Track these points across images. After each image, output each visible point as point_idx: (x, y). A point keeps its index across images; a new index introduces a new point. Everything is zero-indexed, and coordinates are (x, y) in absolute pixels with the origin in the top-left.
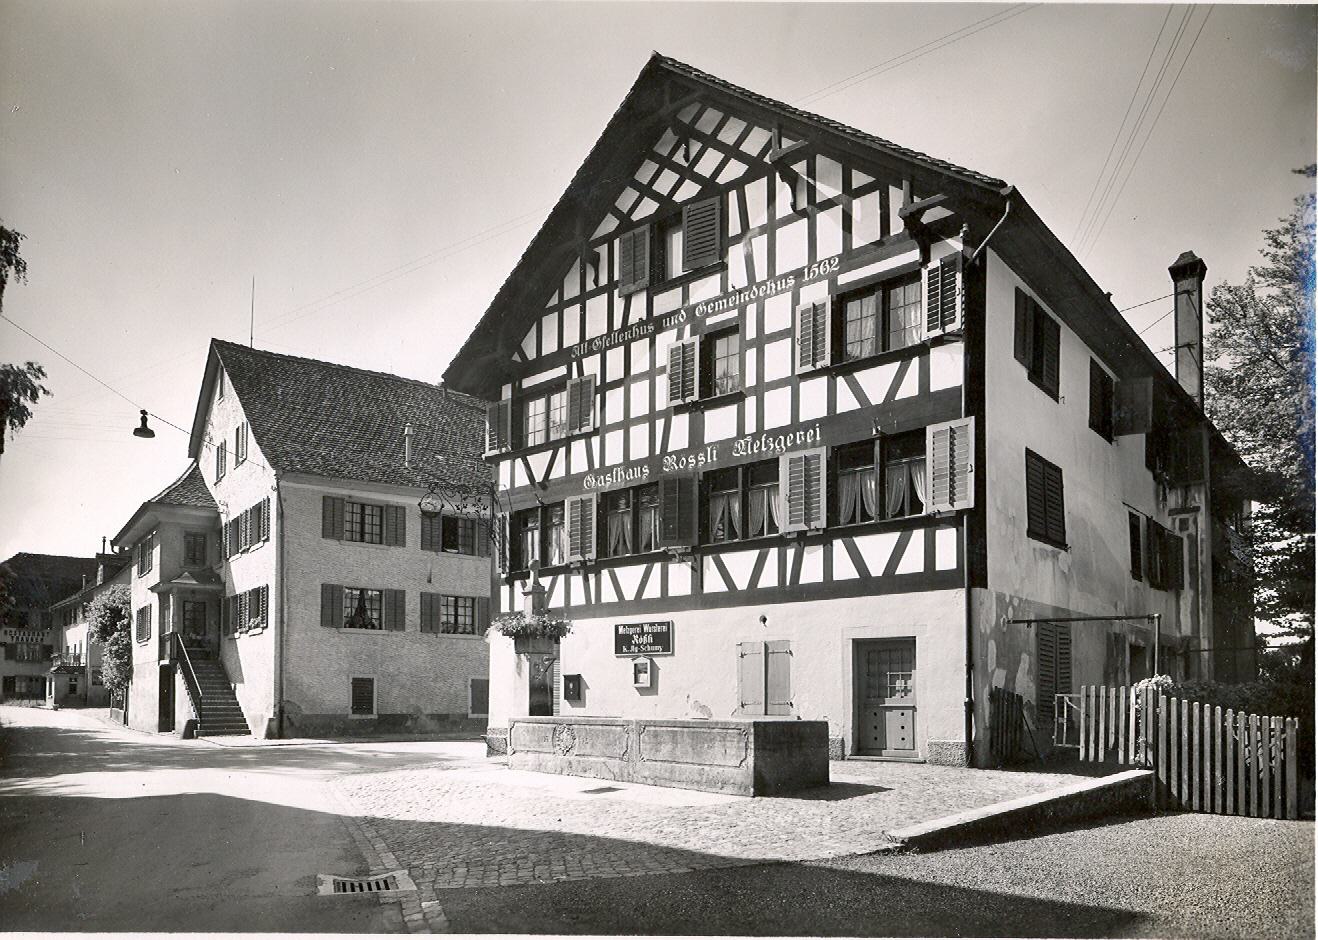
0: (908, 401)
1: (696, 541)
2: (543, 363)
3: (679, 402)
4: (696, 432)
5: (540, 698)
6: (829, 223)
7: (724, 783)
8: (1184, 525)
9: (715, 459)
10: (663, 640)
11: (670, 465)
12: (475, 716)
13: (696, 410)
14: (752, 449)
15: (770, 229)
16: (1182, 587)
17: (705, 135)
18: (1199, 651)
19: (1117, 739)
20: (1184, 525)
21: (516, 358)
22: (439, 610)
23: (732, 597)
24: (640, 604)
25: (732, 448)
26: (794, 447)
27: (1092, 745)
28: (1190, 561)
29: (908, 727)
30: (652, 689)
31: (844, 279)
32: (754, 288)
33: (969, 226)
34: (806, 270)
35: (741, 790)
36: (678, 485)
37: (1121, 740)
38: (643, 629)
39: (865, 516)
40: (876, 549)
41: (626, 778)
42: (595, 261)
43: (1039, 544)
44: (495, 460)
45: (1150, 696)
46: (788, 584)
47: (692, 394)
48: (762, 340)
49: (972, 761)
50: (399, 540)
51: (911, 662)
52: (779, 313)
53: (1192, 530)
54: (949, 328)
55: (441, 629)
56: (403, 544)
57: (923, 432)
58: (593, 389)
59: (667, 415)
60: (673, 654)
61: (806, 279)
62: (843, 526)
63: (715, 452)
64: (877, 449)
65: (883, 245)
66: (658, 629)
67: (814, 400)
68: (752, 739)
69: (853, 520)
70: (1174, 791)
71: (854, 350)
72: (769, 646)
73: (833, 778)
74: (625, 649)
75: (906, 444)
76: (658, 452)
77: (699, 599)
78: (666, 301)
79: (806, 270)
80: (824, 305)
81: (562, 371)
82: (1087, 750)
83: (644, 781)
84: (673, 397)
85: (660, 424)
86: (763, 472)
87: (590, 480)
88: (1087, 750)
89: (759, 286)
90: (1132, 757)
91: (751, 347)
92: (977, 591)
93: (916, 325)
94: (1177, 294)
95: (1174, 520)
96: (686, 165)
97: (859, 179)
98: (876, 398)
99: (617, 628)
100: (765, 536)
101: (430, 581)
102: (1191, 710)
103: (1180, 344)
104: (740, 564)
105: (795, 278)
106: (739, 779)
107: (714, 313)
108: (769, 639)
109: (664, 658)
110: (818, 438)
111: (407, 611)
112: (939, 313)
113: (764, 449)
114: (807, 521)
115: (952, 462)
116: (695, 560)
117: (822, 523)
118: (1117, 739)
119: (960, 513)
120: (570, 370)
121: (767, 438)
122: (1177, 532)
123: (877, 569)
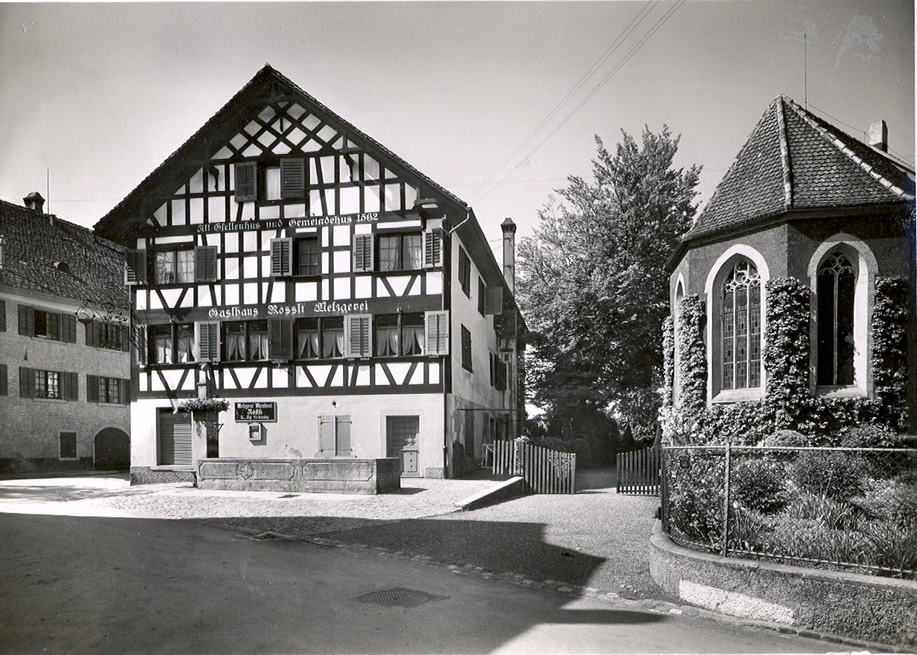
0: (415, 297)
1: (292, 358)
2: (171, 230)
3: (279, 274)
4: (290, 293)
5: (212, 448)
6: (372, 194)
7: (359, 489)
8: (506, 357)
9: (303, 311)
10: (270, 412)
11: (272, 310)
12: (64, 459)
13: (290, 282)
14: (326, 309)
15: (337, 185)
16: (506, 389)
17: (295, 120)
18: (512, 421)
19: (508, 464)
20: (506, 357)
21: (149, 222)
22: (34, 380)
23: (314, 391)
24: (252, 391)
25: (314, 307)
26: (352, 312)
27: (498, 467)
28: (509, 376)
29: (414, 461)
30: (262, 441)
31: (380, 226)
32: (327, 218)
33: (447, 217)
34: (359, 216)
35: (370, 492)
36: (280, 323)
37: (510, 464)
38: (255, 406)
39: (392, 353)
40: (399, 371)
41: (293, 490)
42: (216, 174)
43: (465, 371)
44: (134, 289)
45: (523, 445)
46: (349, 385)
47: (288, 272)
48: (331, 249)
49: (447, 477)
50: (71, 338)
51: (415, 428)
52: (342, 235)
53: (510, 361)
54: (437, 265)
55: (36, 395)
56: (75, 342)
57: (423, 313)
58: (215, 256)
59: (271, 281)
60: (276, 421)
61: (359, 220)
62: (382, 357)
63: (303, 307)
64: (399, 319)
65: (402, 214)
66: (265, 406)
67: (364, 287)
68: (375, 467)
69: (385, 354)
70: (531, 485)
71: (384, 267)
72: (338, 418)
73: (402, 486)
74: (242, 417)
75: (415, 319)
76: (264, 301)
77: (292, 390)
78: (268, 213)
79: (359, 216)
80: (369, 238)
81: (190, 238)
82: (496, 469)
83: (307, 490)
84: (274, 270)
85: (265, 286)
86: (335, 323)
87: (214, 312)
88: (496, 469)
89: (330, 217)
90: (515, 472)
91: (325, 251)
92: (448, 395)
93: (419, 259)
94: (504, 239)
95: (502, 355)
96: (281, 133)
97: (389, 175)
98: (399, 292)
99: (236, 404)
100: (334, 358)
101: (26, 359)
102: (538, 450)
103: (506, 265)
104: (320, 373)
105: (352, 219)
106: (368, 487)
107: (301, 227)
108: (338, 415)
109: (270, 424)
110: (367, 309)
111: (8, 381)
112: (433, 255)
113: (334, 310)
114: (362, 353)
115: (438, 331)
116: (291, 368)
117: (370, 354)
118: (508, 464)
119: (441, 357)
120: (196, 239)
121: (336, 304)
122: (504, 361)
123: (399, 381)
